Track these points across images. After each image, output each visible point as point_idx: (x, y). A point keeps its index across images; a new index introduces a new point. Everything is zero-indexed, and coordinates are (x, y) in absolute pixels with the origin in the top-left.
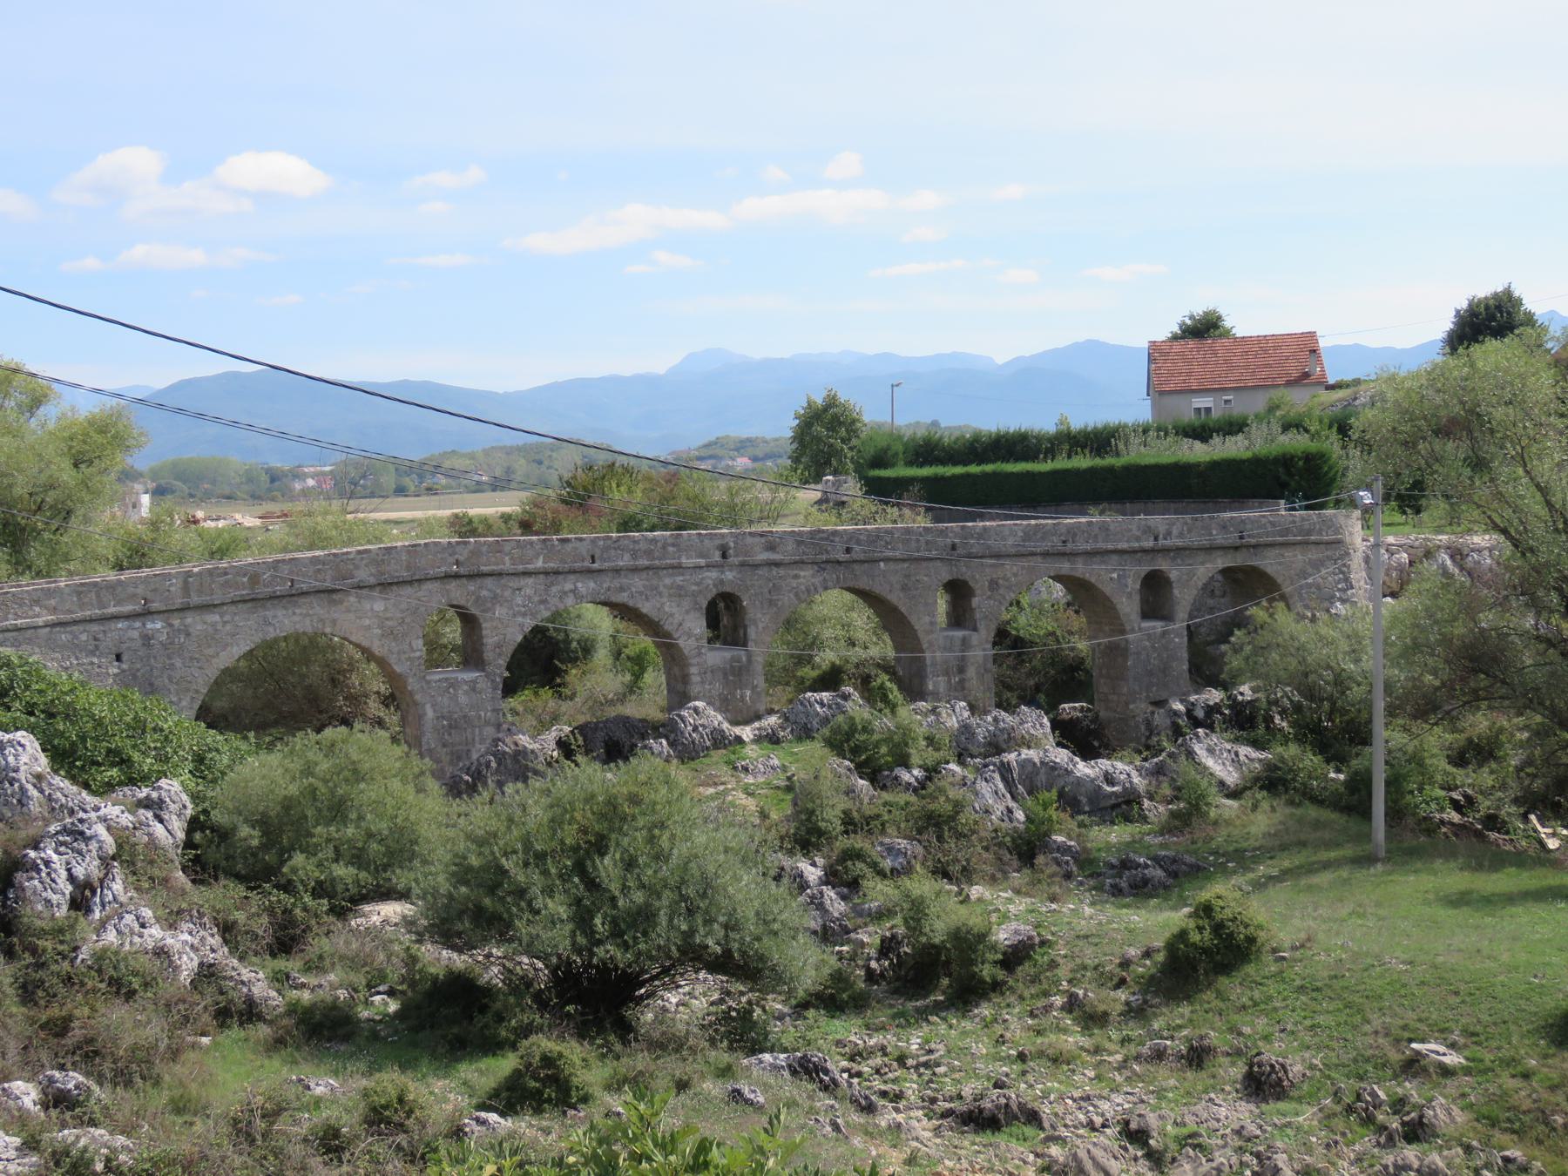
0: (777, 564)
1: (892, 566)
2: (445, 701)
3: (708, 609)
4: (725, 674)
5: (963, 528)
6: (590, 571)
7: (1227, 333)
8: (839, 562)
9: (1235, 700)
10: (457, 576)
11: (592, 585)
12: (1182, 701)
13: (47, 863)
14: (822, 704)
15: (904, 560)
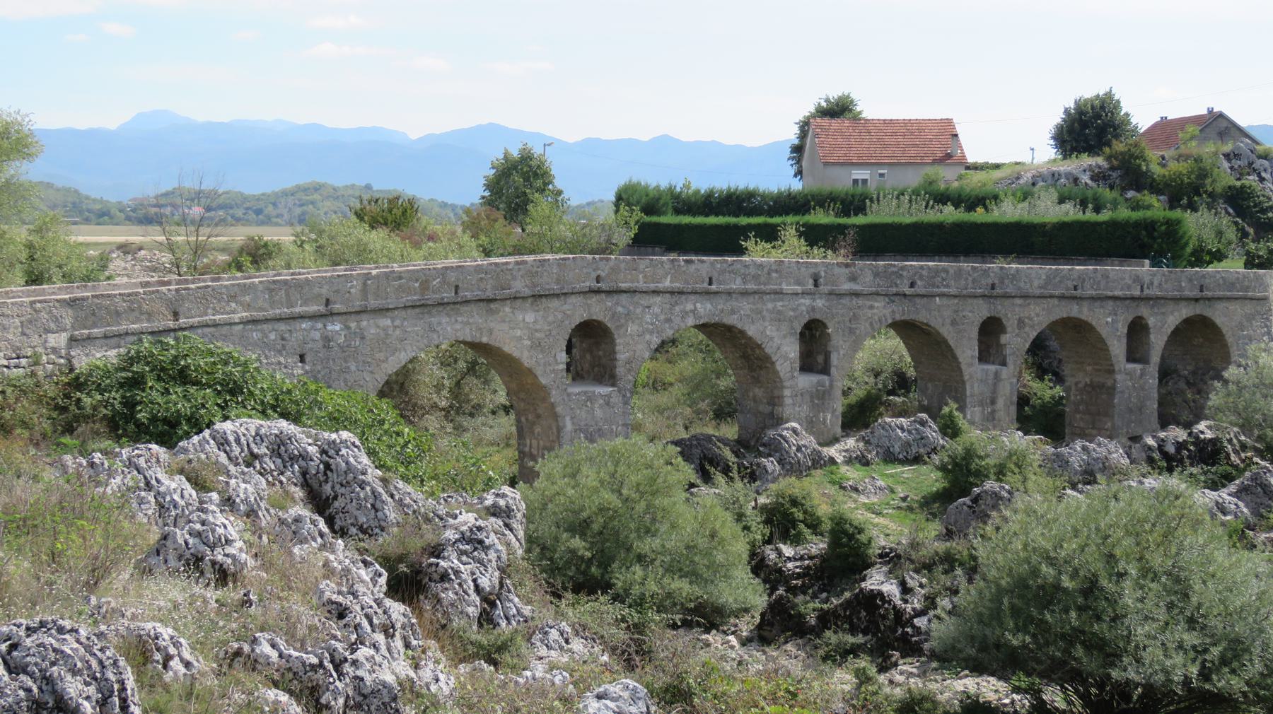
0: (856, 294)
1: (945, 301)
2: (582, 414)
3: (802, 334)
4: (812, 397)
5: (1002, 268)
6: (708, 293)
7: (856, 118)
8: (905, 295)
9: (1197, 438)
10: (598, 292)
11: (709, 306)
12: (1154, 437)
14: (902, 429)
15: (955, 296)
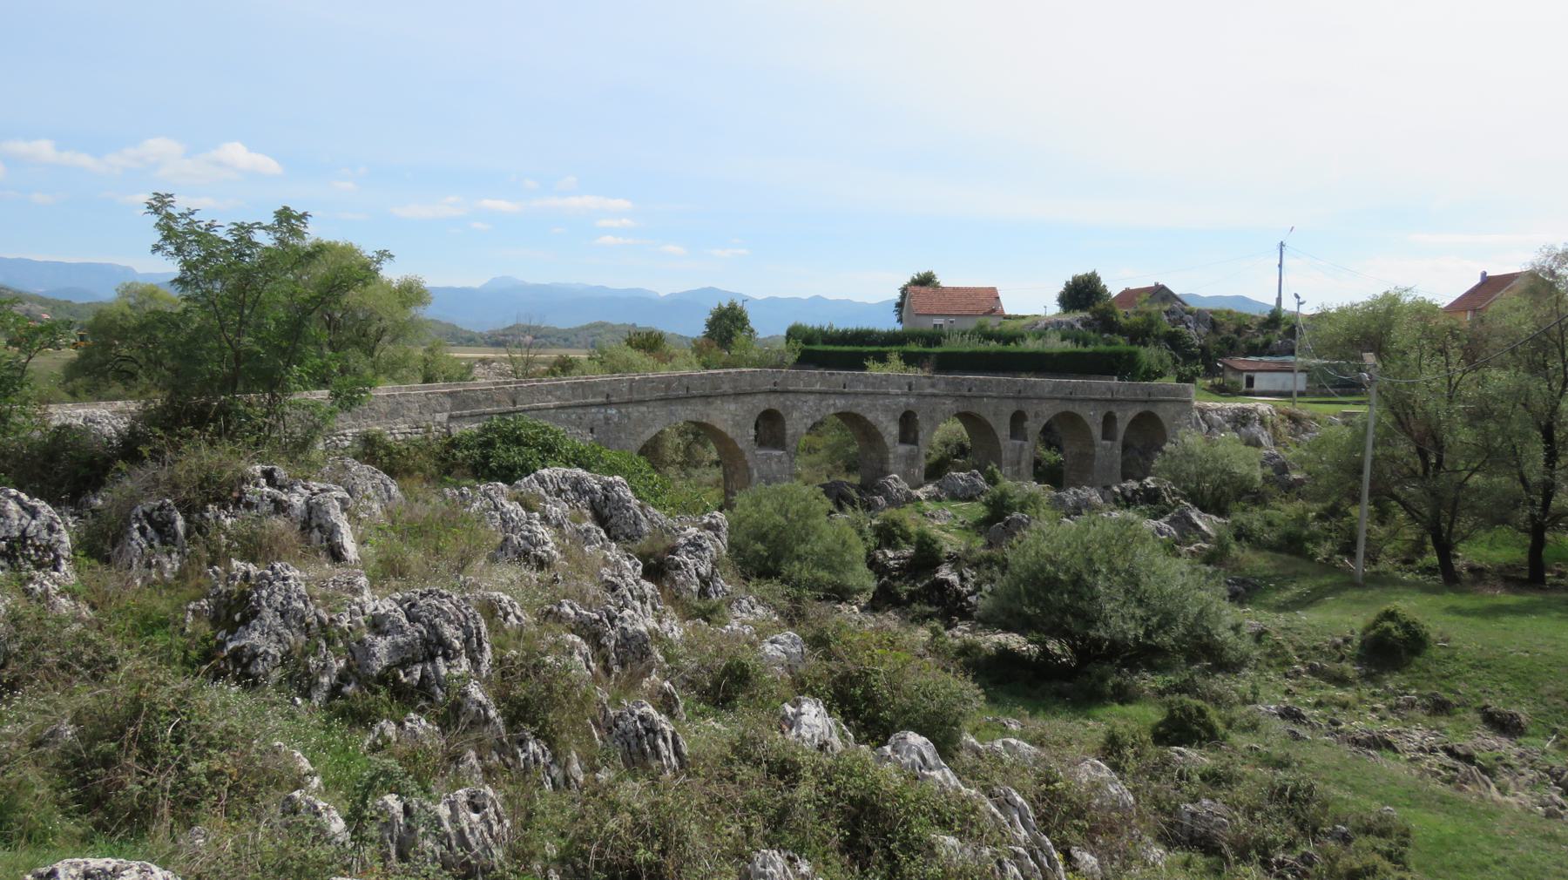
6: (843, 394)
7: (936, 286)
10: (775, 392)
13: (686, 564)
